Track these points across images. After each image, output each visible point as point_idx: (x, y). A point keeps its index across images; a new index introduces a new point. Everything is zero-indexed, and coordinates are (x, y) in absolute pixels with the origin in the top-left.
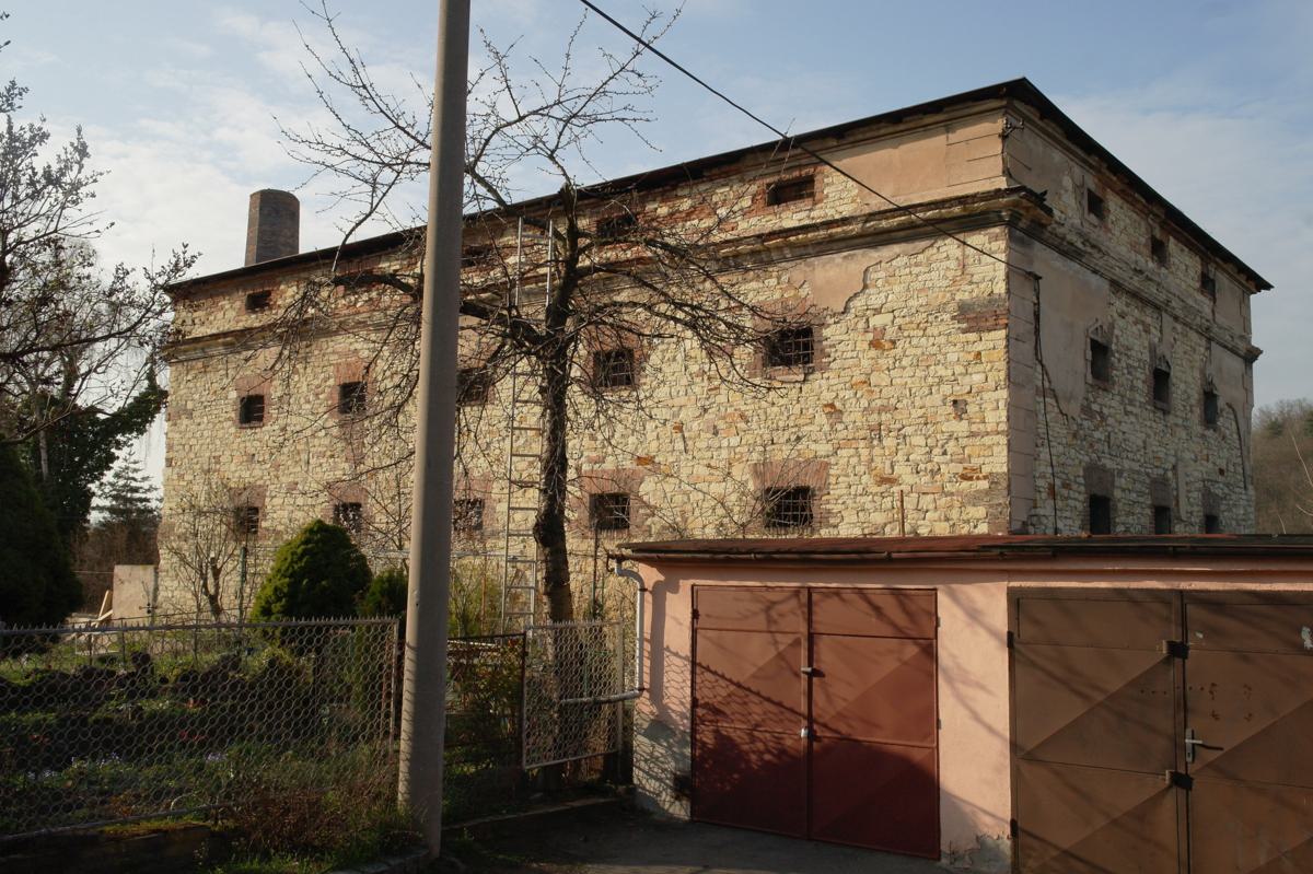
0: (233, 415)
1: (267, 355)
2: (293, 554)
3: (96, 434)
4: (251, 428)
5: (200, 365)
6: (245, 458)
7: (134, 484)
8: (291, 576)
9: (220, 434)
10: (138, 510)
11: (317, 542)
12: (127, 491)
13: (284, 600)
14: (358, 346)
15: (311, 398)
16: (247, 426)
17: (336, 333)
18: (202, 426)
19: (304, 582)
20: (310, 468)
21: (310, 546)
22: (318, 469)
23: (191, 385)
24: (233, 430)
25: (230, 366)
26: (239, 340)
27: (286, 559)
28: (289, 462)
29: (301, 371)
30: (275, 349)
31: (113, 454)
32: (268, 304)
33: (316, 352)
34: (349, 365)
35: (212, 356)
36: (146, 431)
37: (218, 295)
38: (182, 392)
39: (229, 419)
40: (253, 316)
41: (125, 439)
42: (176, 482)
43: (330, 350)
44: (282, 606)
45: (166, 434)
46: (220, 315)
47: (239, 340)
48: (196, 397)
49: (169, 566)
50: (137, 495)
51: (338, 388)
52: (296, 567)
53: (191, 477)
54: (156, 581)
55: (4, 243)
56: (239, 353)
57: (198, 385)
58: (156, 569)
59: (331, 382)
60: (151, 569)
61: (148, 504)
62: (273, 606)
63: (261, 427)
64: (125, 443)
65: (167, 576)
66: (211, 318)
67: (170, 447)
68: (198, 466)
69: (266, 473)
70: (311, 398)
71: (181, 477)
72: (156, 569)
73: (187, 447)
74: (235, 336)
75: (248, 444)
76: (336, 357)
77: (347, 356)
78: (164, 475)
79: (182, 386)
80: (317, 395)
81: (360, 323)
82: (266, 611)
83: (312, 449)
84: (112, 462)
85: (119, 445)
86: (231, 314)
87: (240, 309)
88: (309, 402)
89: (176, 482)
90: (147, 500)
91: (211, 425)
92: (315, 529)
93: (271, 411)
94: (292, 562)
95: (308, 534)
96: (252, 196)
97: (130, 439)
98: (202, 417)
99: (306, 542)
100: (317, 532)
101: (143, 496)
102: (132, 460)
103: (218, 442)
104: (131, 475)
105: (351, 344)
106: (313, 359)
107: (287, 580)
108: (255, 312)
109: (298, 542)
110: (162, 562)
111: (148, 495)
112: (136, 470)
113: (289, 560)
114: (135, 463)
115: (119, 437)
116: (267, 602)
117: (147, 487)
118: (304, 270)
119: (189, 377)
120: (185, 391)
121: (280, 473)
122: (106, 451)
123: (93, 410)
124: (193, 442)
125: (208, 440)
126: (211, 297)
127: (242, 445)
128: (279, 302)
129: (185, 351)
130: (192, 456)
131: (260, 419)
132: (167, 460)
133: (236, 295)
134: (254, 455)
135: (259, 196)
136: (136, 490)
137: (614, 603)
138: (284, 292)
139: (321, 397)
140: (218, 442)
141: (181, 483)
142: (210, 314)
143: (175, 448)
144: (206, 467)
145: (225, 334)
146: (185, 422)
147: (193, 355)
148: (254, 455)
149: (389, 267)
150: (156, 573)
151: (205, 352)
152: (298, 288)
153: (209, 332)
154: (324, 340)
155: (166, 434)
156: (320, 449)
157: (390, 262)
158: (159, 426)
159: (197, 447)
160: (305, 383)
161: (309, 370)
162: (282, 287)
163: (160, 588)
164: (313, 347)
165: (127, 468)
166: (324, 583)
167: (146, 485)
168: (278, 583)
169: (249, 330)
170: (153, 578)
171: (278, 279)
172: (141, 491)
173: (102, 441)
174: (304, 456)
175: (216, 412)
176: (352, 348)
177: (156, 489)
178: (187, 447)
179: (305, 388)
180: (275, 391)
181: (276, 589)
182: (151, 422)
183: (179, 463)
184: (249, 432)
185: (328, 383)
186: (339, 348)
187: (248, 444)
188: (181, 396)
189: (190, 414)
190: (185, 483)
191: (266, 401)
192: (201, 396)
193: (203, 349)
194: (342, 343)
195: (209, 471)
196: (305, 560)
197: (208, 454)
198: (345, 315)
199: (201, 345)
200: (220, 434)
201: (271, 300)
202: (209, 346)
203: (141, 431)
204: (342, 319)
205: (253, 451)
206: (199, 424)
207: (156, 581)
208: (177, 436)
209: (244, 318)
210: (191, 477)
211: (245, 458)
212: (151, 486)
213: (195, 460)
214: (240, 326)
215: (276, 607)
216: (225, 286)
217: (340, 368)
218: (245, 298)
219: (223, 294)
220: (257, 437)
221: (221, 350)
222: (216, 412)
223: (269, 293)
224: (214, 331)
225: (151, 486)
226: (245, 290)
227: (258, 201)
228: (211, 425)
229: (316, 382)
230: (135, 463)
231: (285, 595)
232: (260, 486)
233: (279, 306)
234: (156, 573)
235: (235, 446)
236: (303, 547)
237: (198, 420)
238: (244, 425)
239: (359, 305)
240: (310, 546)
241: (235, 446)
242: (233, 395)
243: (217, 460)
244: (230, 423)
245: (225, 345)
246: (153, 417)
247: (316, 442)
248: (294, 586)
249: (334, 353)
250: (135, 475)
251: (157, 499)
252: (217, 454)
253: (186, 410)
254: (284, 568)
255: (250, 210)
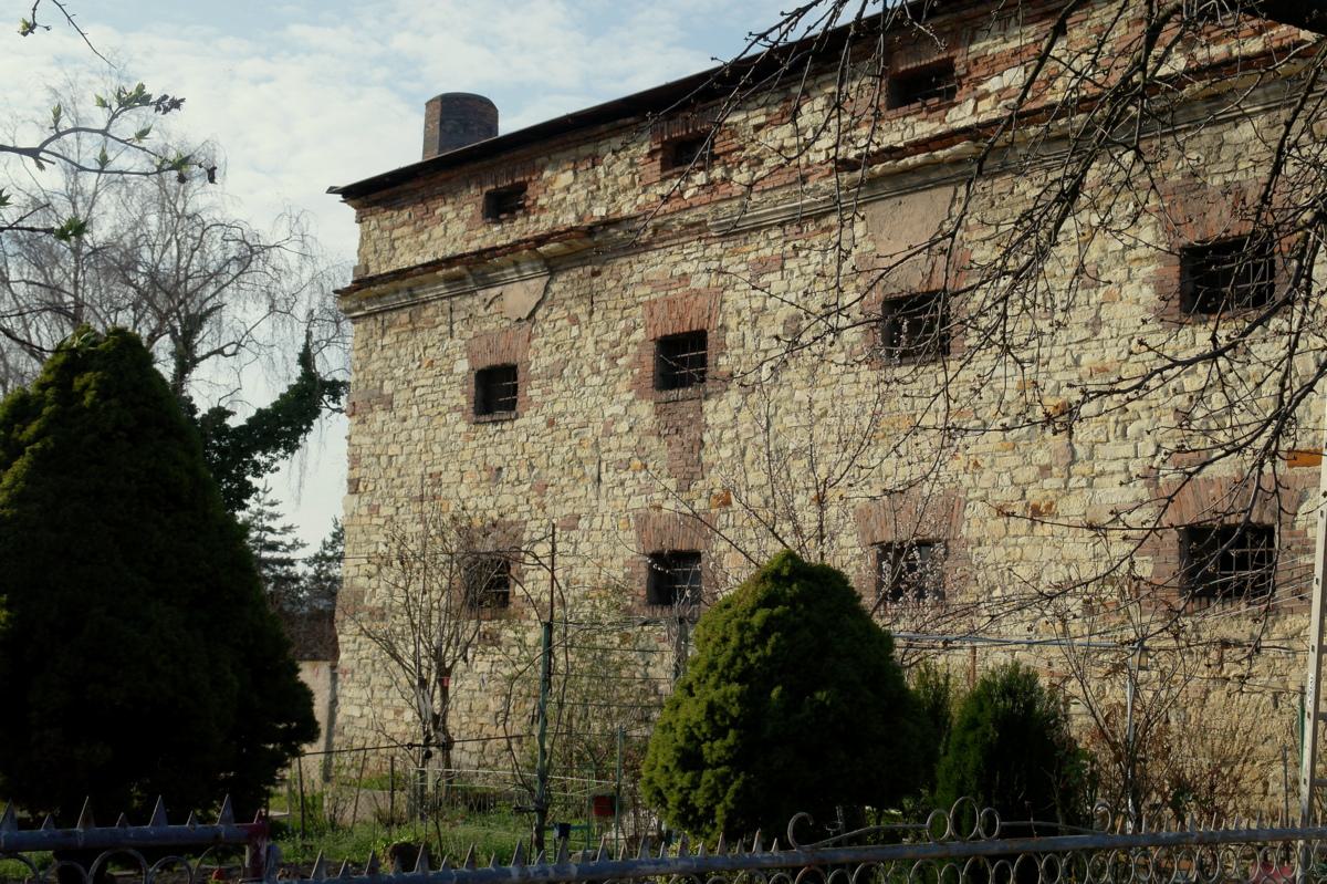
0: (463, 402)
1: (519, 295)
2: (741, 627)
3: (222, 451)
4: (495, 422)
5: (404, 317)
6: (485, 475)
7: (270, 538)
8: (740, 679)
9: (441, 434)
10: (277, 578)
11: (793, 602)
12: (261, 548)
13: (732, 733)
14: (688, 268)
15: (603, 365)
16: (488, 418)
17: (647, 246)
18: (409, 423)
19: (775, 693)
20: (603, 489)
21: (779, 610)
22: (618, 491)
23: (390, 353)
24: (462, 427)
25: (456, 317)
26: (473, 271)
27: (725, 640)
28: (564, 481)
29: (584, 318)
30: (537, 284)
31: (250, 483)
32: (522, 207)
33: (611, 284)
34: (671, 302)
35: (425, 302)
36: (298, 446)
37: (433, 198)
38: (374, 366)
39: (455, 408)
40: (496, 229)
41: (267, 460)
42: (365, 520)
43: (636, 278)
44: (729, 749)
45: (349, 438)
46: (438, 231)
47: (473, 271)
48: (399, 373)
49: (355, 662)
50: (277, 555)
51: (653, 346)
52: (752, 658)
53: (392, 511)
54: (334, 688)
55: (5, 392)
56: (472, 293)
57: (402, 351)
58: (333, 667)
59: (639, 335)
60: (324, 667)
61: (292, 569)
62: (705, 747)
63: (512, 420)
64: (267, 466)
65: (352, 679)
66: (424, 237)
67: (355, 461)
68: (403, 491)
69: (521, 499)
70: (603, 365)
71: (374, 510)
72: (333, 667)
73: (384, 459)
74: (467, 264)
75: (490, 450)
76: (648, 290)
77: (668, 286)
78: (345, 508)
79: (374, 356)
80: (613, 359)
81: (693, 225)
82: (690, 760)
83: (604, 456)
84: (248, 497)
85: (258, 470)
86: (457, 228)
87: (473, 216)
88: (598, 372)
89: (365, 520)
90: (291, 562)
91: (424, 421)
92: (785, 572)
93: (531, 391)
94: (742, 646)
95: (769, 584)
96: (428, 104)
97: (273, 460)
98: (409, 407)
99: (769, 601)
100: (789, 580)
101: (285, 556)
102: (268, 500)
103: (437, 449)
104: (266, 523)
105: (675, 264)
106: (605, 296)
107: (735, 688)
108: (500, 222)
109: (750, 602)
110: (343, 656)
111: (292, 555)
112: (273, 516)
113: (734, 642)
114: (273, 504)
115: (258, 457)
116: (691, 737)
117: (289, 542)
118: (587, 141)
119: (387, 341)
120: (379, 364)
121: (548, 500)
122: (240, 478)
123: (220, 414)
124: (395, 449)
125: (420, 446)
126: (423, 200)
127: (479, 453)
128: (543, 201)
129: (380, 296)
130: (393, 473)
131: (511, 406)
132: (350, 482)
133: (464, 196)
134: (500, 469)
135: (439, 103)
136: (273, 547)
137: (1271, 751)
138: (550, 182)
139: (620, 362)
140: (437, 449)
141: (375, 521)
142: (421, 230)
143: (366, 461)
144: (417, 493)
145: (449, 261)
146: (380, 416)
147: (392, 301)
148: (500, 469)
149: (747, 119)
150: (334, 677)
151: (412, 296)
152: (575, 174)
153: (420, 260)
154: (624, 260)
155: (349, 438)
156: (620, 455)
157: (748, 111)
158: (330, 433)
159: (402, 459)
160: (591, 341)
161: (597, 317)
162: (547, 174)
163: (341, 701)
164: (606, 274)
165: (261, 513)
166: (820, 695)
167: (288, 539)
168: (715, 695)
169: (493, 251)
170: (328, 683)
171: (539, 161)
172: (281, 548)
173: (233, 463)
174: (591, 469)
175: (432, 397)
176: (677, 271)
177: (303, 545)
178: (384, 459)
179: (590, 347)
180: (538, 360)
181: (711, 708)
182: (306, 432)
183: (371, 487)
184: (491, 429)
185: (632, 338)
186: (653, 272)
187: (490, 450)
188: (374, 373)
189: (388, 404)
190: (381, 521)
191: (521, 376)
192: (407, 371)
193: (410, 290)
194: (658, 264)
195: (421, 499)
196: (772, 640)
197: (419, 471)
198: (665, 214)
199: (407, 283)
200: (441, 434)
201: (527, 198)
202: (421, 285)
203: (292, 447)
204: (658, 220)
205: (498, 462)
206: (404, 420)
207: (334, 688)
208: (368, 440)
209: (479, 234)
210: (392, 511)
211: (485, 475)
212: (295, 541)
213: (398, 482)
214: (474, 246)
215: (714, 750)
216: (447, 180)
217: (656, 309)
218: (481, 199)
219: (443, 195)
220: (504, 437)
221: (442, 289)
222: (432, 397)
223: (522, 187)
224: (429, 258)
225: (295, 541)
226: (481, 185)
227: (438, 111)
228: (424, 421)
229: (611, 337)
230: (273, 504)
231: (734, 723)
232: (512, 523)
233: (542, 208)
234: (334, 677)
235: (467, 455)
236: (762, 614)
237: (402, 413)
238: (482, 418)
239: (687, 195)
240: (779, 610)
241: (467, 455)
242: (462, 366)
243: (437, 479)
244: (457, 415)
245: (449, 280)
246: (310, 424)
247: (613, 443)
248: (753, 700)
249: (643, 282)
250: (271, 524)
251: (305, 561)
252: (436, 469)
253: (381, 396)
254: (722, 661)
255: (426, 126)
